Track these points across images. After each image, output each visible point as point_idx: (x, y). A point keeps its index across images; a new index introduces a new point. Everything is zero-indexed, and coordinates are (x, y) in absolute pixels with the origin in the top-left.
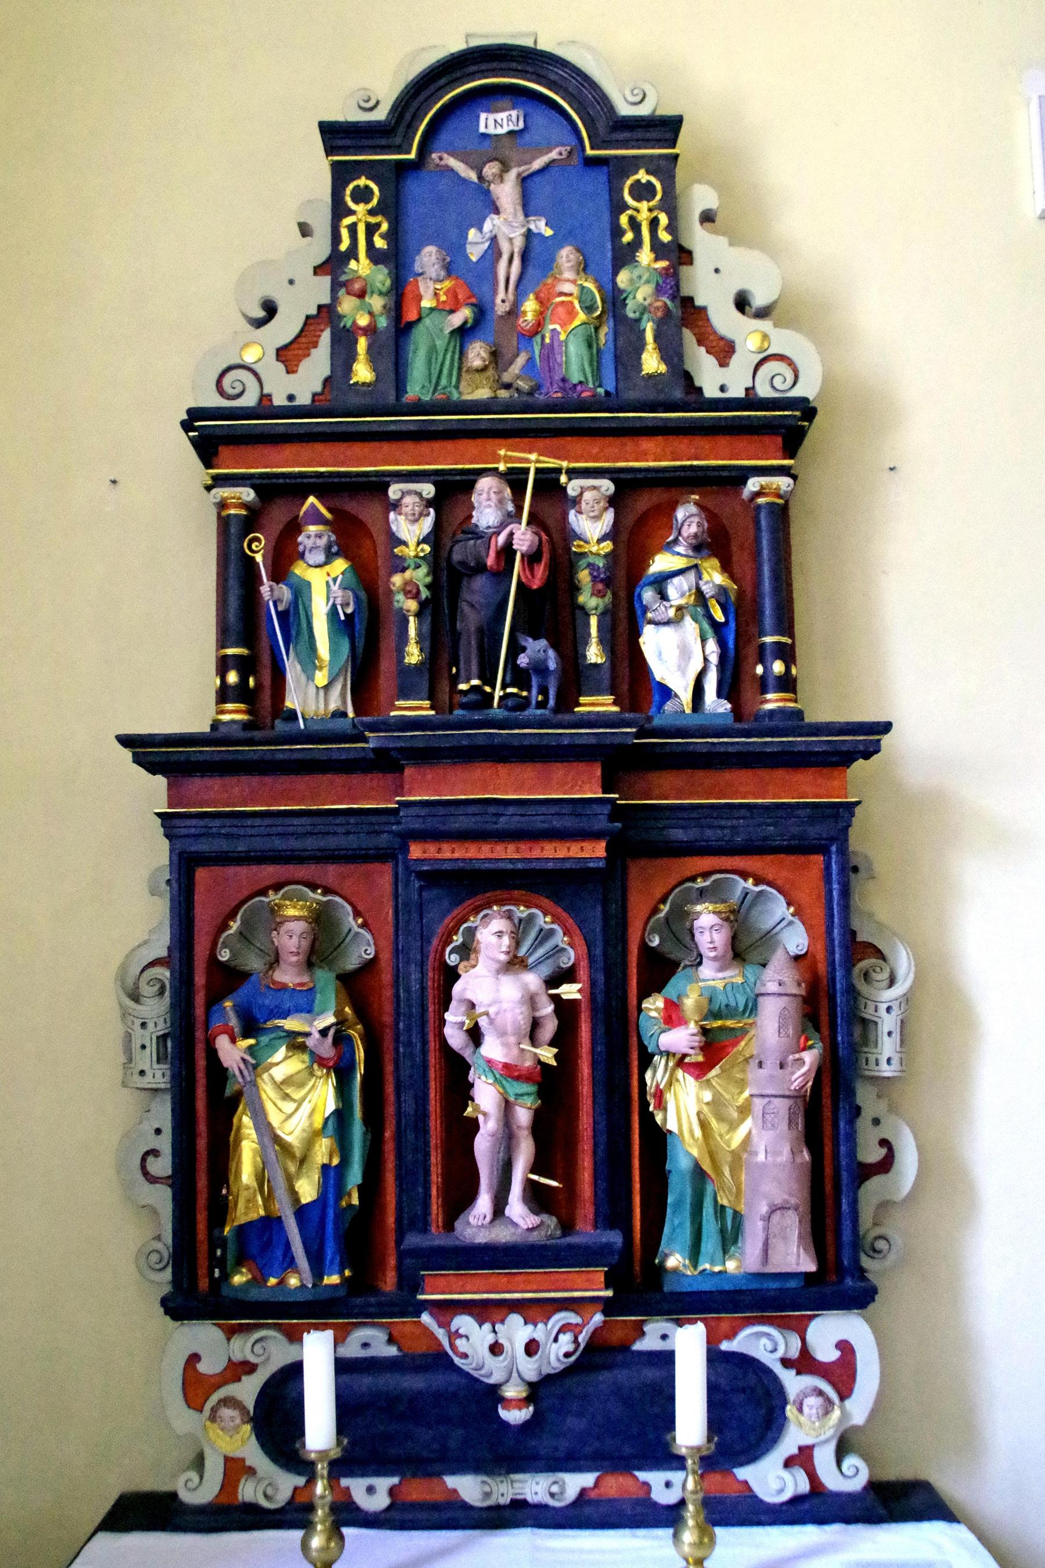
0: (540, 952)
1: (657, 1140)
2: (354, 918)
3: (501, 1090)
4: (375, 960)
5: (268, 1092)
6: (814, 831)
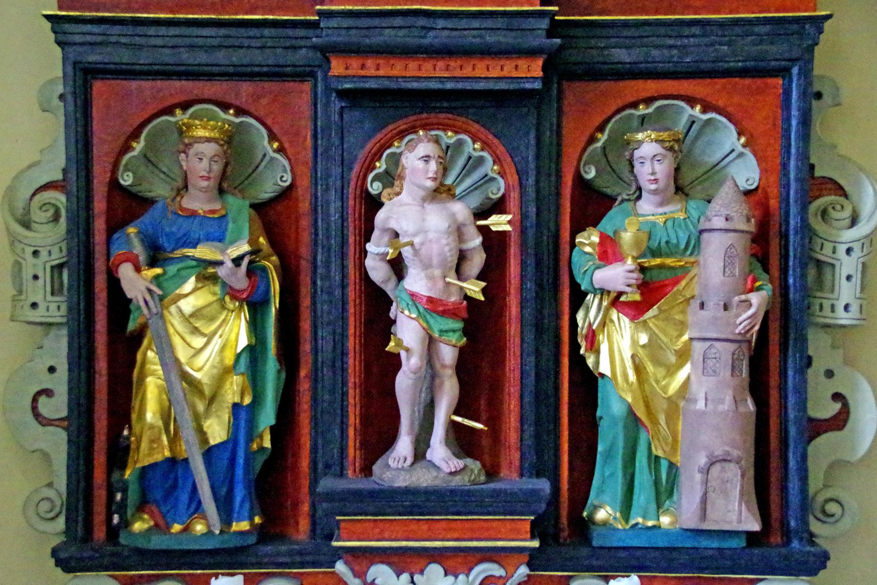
0: (468, 182)
1: (587, 383)
2: (269, 142)
3: (425, 325)
4: (291, 187)
5: (175, 324)
6: (777, 50)
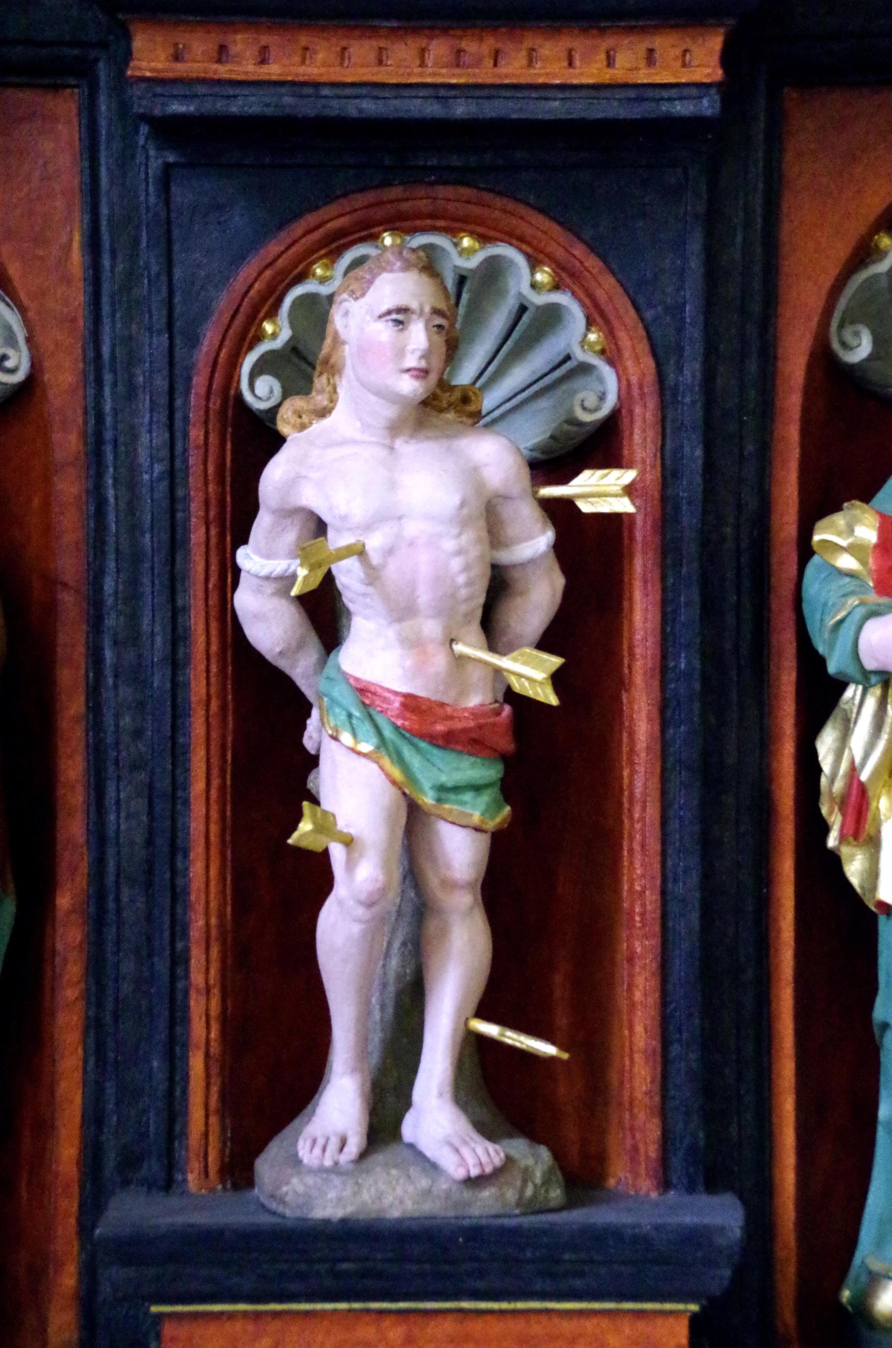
0: (518, 376)
3: (397, 774)
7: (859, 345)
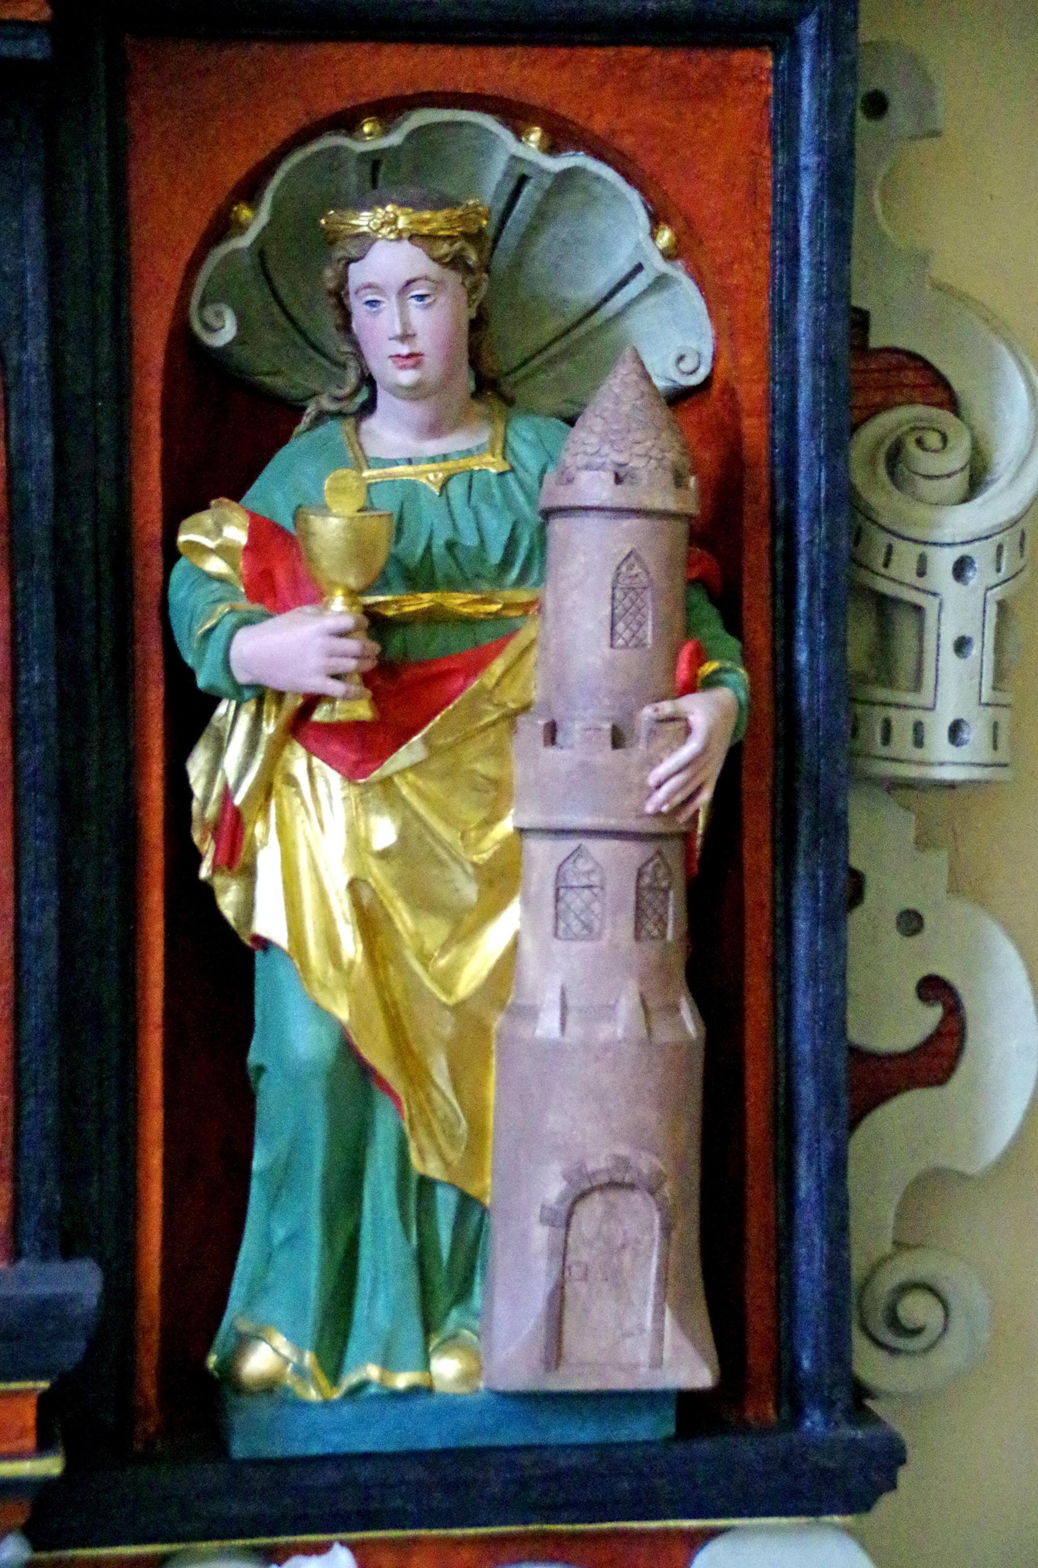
7: (223, 327)
